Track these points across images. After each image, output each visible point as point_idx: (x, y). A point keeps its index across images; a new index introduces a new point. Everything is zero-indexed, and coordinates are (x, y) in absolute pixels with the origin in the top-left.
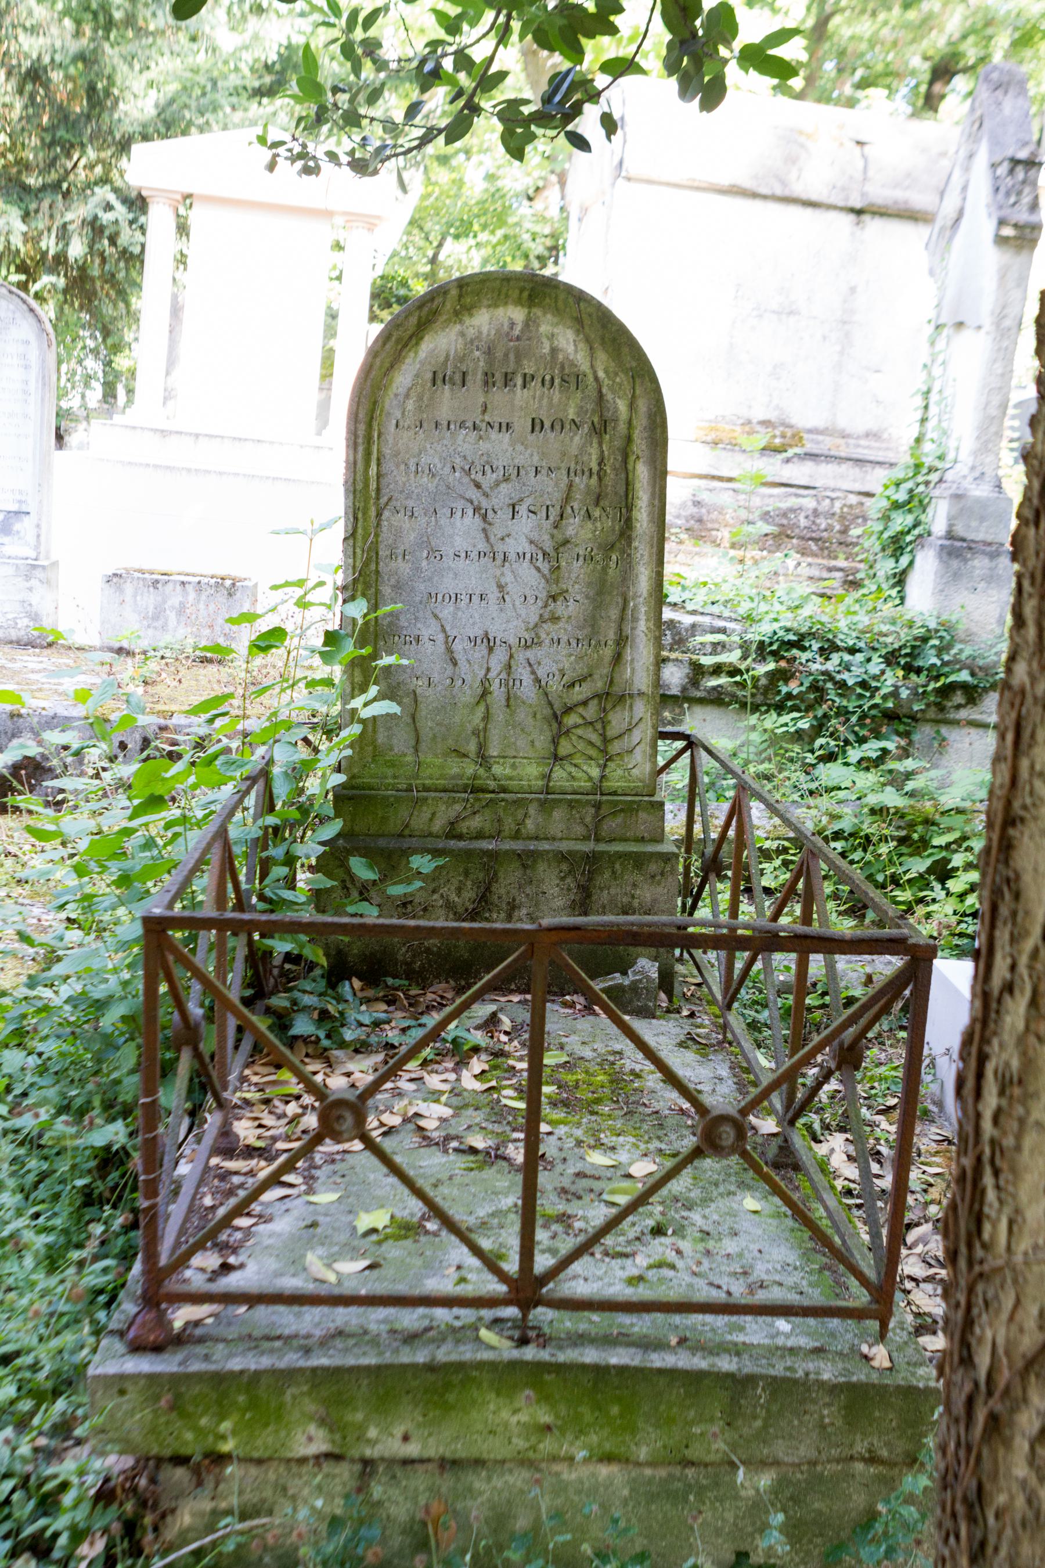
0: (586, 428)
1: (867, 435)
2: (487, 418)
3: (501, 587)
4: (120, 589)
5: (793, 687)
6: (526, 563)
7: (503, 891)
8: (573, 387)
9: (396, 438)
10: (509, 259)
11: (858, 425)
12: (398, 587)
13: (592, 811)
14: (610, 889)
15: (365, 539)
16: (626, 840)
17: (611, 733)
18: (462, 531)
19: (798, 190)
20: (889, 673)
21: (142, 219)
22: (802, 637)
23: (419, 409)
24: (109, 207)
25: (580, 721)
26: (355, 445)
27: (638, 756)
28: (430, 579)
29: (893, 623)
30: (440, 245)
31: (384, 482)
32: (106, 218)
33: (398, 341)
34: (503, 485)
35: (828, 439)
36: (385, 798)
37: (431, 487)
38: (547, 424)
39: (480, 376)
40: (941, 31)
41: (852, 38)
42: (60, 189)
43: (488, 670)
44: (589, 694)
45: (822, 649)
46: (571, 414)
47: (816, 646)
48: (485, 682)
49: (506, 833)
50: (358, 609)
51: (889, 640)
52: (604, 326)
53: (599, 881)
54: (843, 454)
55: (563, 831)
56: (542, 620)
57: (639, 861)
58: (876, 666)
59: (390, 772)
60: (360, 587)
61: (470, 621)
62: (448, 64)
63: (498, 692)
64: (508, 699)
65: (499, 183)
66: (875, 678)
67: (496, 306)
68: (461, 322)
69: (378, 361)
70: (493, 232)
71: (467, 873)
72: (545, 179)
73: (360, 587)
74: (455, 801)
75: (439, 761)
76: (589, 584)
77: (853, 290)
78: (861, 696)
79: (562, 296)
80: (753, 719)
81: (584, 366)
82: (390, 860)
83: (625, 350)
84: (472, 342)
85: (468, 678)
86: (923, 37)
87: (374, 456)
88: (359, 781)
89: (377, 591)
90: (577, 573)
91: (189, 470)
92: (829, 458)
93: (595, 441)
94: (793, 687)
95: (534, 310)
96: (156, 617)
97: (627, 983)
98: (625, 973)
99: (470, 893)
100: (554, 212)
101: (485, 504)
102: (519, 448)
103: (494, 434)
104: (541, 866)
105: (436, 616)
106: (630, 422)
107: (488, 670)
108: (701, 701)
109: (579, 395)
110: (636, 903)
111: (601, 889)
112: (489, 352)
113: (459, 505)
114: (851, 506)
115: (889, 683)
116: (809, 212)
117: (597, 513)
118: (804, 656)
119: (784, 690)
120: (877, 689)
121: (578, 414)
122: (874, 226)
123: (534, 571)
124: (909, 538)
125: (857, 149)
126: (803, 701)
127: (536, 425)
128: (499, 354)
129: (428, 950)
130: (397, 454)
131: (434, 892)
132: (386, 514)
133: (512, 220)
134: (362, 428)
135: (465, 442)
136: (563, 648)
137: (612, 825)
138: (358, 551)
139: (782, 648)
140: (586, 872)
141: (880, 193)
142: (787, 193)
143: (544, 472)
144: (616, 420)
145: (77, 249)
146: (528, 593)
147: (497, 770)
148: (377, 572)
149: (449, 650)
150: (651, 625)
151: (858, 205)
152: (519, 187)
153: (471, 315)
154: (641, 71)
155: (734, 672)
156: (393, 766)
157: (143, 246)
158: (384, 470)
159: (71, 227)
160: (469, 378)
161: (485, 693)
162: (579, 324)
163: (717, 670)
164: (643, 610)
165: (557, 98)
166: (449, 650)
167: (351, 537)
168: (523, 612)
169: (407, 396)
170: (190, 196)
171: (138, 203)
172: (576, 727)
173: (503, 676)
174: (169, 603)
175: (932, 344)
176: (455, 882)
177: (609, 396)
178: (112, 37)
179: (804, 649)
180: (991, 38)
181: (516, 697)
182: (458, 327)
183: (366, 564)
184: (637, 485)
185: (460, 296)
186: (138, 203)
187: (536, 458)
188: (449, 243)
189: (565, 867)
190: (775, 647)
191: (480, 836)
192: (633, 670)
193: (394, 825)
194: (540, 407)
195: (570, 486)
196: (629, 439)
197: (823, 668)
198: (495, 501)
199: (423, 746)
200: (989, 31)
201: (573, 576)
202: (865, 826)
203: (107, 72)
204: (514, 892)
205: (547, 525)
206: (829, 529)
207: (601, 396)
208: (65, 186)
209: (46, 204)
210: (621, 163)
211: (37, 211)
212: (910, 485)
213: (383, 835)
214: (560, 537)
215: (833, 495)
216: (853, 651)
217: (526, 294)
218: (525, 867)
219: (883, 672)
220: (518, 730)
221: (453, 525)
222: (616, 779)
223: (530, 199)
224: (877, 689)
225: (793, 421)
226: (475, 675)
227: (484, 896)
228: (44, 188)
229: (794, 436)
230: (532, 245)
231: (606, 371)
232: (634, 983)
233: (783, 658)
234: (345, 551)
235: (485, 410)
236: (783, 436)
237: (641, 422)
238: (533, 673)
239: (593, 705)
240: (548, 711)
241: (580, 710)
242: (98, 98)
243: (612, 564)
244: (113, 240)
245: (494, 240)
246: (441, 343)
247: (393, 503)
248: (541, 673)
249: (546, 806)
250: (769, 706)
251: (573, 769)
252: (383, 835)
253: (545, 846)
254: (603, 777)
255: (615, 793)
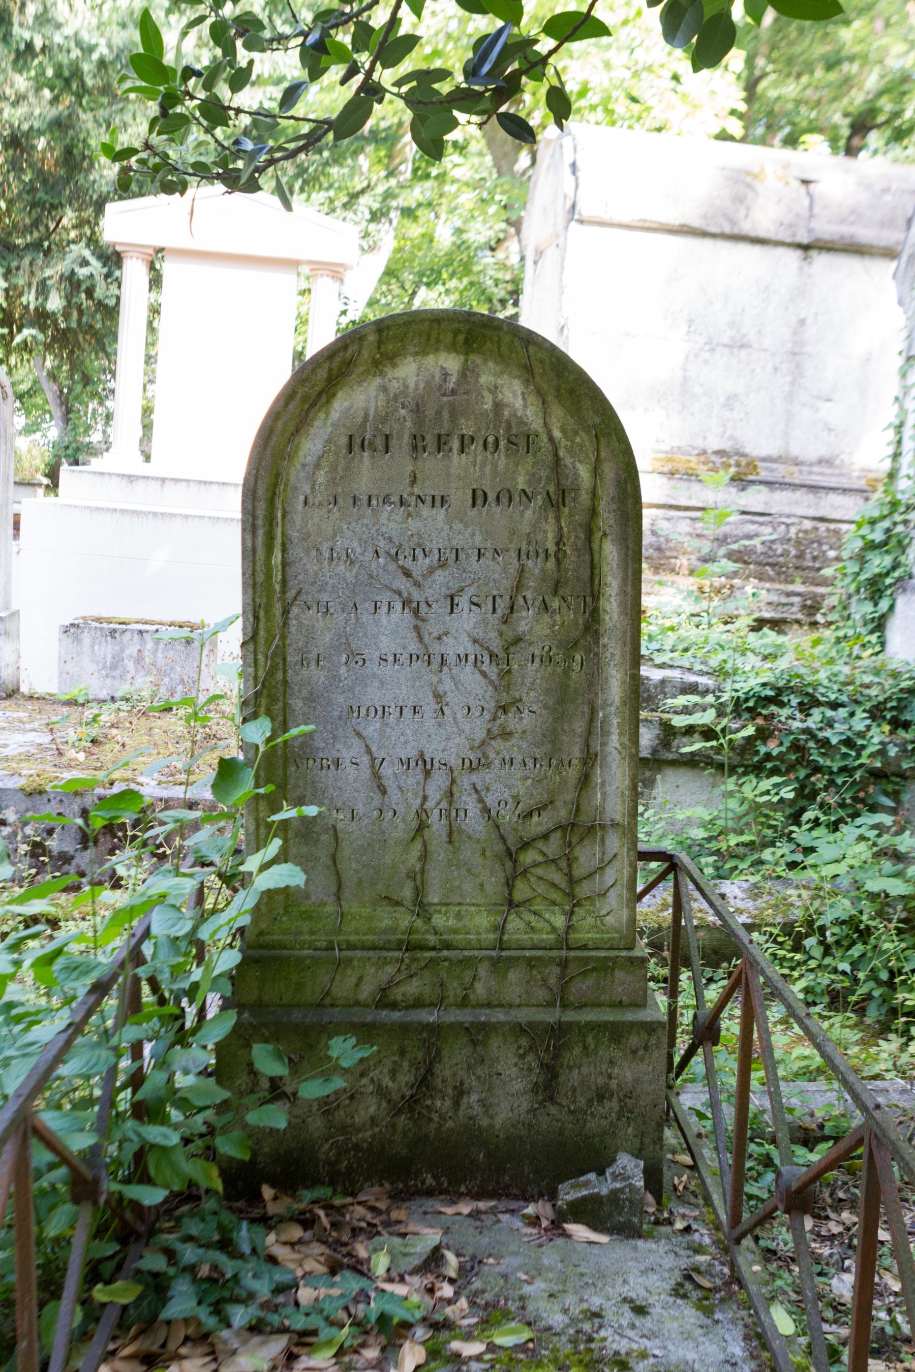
0: (540, 500)
1: (820, 462)
2: (416, 491)
3: (438, 697)
4: (78, 640)
5: (772, 747)
6: (469, 668)
7: (447, 1073)
8: (522, 449)
9: (304, 519)
10: (474, 303)
11: (812, 453)
12: (311, 699)
13: (557, 970)
14: (582, 1071)
15: (268, 643)
16: (598, 1005)
17: (578, 872)
18: (389, 630)
19: (746, 227)
20: (874, 730)
21: (117, 273)
22: (780, 691)
23: (333, 481)
24: (85, 263)
25: (540, 859)
26: (254, 528)
27: (613, 900)
28: (351, 689)
29: (877, 672)
30: (414, 293)
31: (290, 571)
32: (82, 272)
33: (304, 399)
34: (439, 572)
35: (781, 467)
36: (300, 960)
37: (350, 576)
38: (491, 496)
39: (406, 439)
40: (860, 88)
41: (778, 98)
42: (45, 248)
43: (425, 798)
44: (551, 826)
45: (801, 704)
46: (521, 482)
47: (795, 701)
48: (422, 813)
49: (451, 1000)
50: (259, 732)
51: (873, 692)
52: (559, 375)
53: (568, 1058)
54: (797, 481)
55: (520, 998)
56: (490, 735)
57: (616, 1033)
58: (860, 722)
59: (306, 926)
60: (264, 701)
61: (402, 740)
62: (344, 37)
63: (437, 826)
64: (450, 834)
65: (465, 236)
66: (861, 734)
67: (425, 353)
68: (382, 374)
69: (279, 425)
70: (460, 279)
71: (402, 1052)
72: (505, 231)
73: (264, 701)
74: (386, 962)
75: (366, 911)
76: (547, 691)
77: (802, 322)
78: (845, 756)
79: (507, 339)
80: (731, 784)
81: (536, 425)
82: (303, 1040)
83: (586, 404)
84: (396, 397)
85: (401, 809)
86: (843, 96)
87: (279, 540)
88: (268, 938)
89: (286, 706)
90: (531, 677)
91: (155, 514)
92: (783, 485)
93: (551, 515)
94: (772, 747)
95: (472, 357)
96: (114, 667)
97: (605, 1191)
98: (601, 1172)
99: (406, 1077)
100: (514, 260)
101: (416, 596)
102: (458, 526)
103: (425, 511)
104: (495, 1042)
105: (359, 735)
106: (594, 492)
107: (425, 798)
108: (673, 763)
109: (530, 459)
110: (613, 1084)
111: (570, 1068)
112: (417, 409)
113: (384, 597)
114: (806, 532)
115: (876, 740)
116: (757, 249)
117: (555, 603)
118: (785, 712)
119: (763, 750)
120: (863, 747)
121: (529, 483)
122: (821, 260)
123: (478, 676)
124: (888, 581)
125: (803, 189)
126: (782, 761)
127: (478, 498)
128: (430, 413)
129: (356, 1147)
130: (306, 537)
131: (362, 1075)
132: (295, 610)
133: (477, 268)
134: (261, 507)
135: (390, 521)
136: (517, 772)
137: (581, 987)
138: (261, 657)
139: (757, 706)
140: (549, 1045)
141: (826, 229)
142: (736, 231)
143: (489, 554)
144: (577, 490)
145: (55, 303)
146: (472, 704)
147: (438, 921)
148: (285, 682)
149: (376, 776)
150: (626, 740)
151: (805, 240)
152: (482, 239)
153: (394, 366)
154: (601, 30)
155: (708, 733)
156: (310, 918)
157: (118, 298)
158: (291, 556)
159: (49, 282)
160: (393, 442)
161: (421, 827)
162: (528, 372)
163: (690, 730)
164: (615, 722)
165: (486, 68)
166: (376, 776)
167: (250, 641)
168: (467, 727)
169: (317, 466)
170: (162, 250)
171: (113, 259)
172: (536, 865)
173: (444, 805)
174: (127, 652)
175: (904, 375)
176: (388, 1063)
177: (568, 461)
178: (84, 102)
179: (782, 705)
180: (904, 93)
181: (460, 831)
182: (378, 381)
183: (271, 673)
184: (605, 569)
185: (380, 343)
186: (113, 259)
187: (478, 538)
188: (423, 292)
189: (524, 1042)
190: (751, 704)
191: (418, 1003)
192: (604, 794)
193: (311, 993)
194: (483, 475)
195: (522, 571)
196: (593, 512)
197: (804, 725)
198: (429, 592)
199: (347, 893)
200: (906, 87)
201: (528, 681)
202: (865, 917)
203: (82, 137)
204: (462, 1073)
205: (494, 620)
206: (785, 554)
207: (557, 460)
208: (46, 244)
209: (26, 261)
210: (573, 207)
211: (18, 268)
212: (886, 524)
213: (298, 1005)
214: (510, 634)
215: (789, 521)
216: (835, 706)
217: (461, 338)
218: (474, 1043)
219: (869, 728)
220: (463, 872)
221: (377, 623)
222: (586, 930)
223: (492, 249)
224: (863, 747)
225: (747, 450)
226: (409, 806)
227: (424, 1079)
228: (27, 246)
229: (748, 465)
230: (496, 290)
231: (563, 430)
232: (615, 1193)
233: (760, 714)
234: (244, 657)
235: (414, 480)
236: (738, 465)
237: (608, 491)
238: (481, 801)
239: (556, 839)
240: (500, 848)
241: (540, 844)
242: (74, 160)
243: (576, 667)
244: (90, 293)
245: (461, 287)
246: (357, 400)
247: (303, 597)
248: (490, 800)
249: (499, 966)
250: (746, 767)
251: (532, 918)
252: (298, 1005)
253: (499, 1016)
254: (569, 928)
255: (584, 947)
